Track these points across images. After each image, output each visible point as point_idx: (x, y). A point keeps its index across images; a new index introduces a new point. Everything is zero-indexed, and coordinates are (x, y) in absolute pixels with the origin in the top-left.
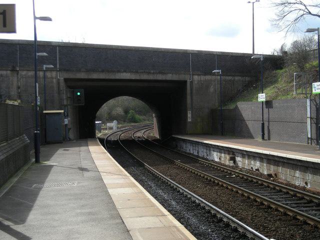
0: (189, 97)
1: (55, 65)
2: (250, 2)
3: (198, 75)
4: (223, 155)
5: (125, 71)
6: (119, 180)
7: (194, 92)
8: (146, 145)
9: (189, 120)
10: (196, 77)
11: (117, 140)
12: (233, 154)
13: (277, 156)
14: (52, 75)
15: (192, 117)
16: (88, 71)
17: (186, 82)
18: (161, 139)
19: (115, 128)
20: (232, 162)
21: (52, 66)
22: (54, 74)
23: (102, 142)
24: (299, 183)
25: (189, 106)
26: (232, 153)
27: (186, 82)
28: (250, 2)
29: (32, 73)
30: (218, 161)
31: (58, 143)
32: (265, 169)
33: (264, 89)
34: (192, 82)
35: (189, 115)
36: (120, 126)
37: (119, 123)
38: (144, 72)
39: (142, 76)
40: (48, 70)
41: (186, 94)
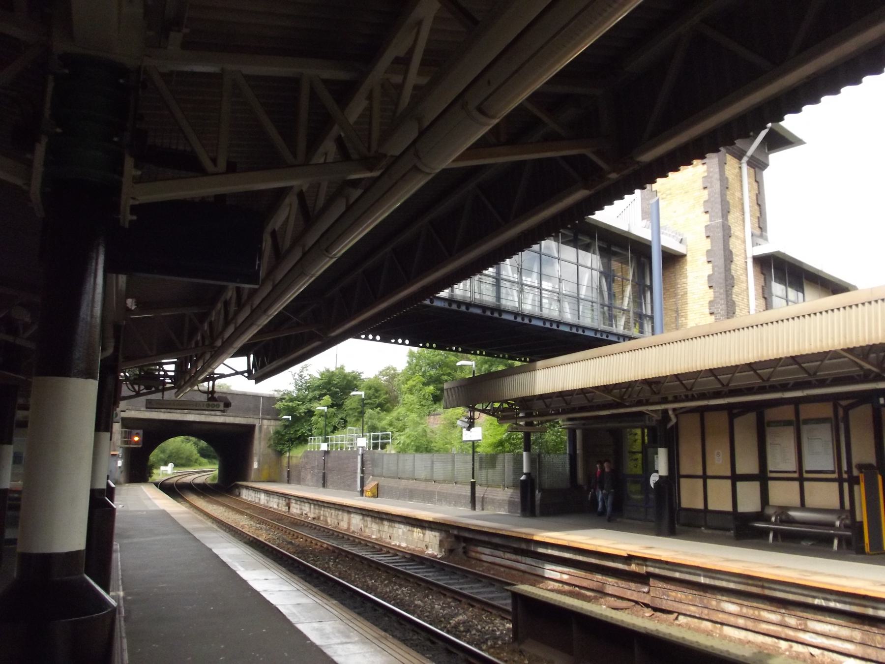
4: (281, 501)
8: (202, 490)
10: (265, 422)
24: (344, 525)
34: (261, 427)
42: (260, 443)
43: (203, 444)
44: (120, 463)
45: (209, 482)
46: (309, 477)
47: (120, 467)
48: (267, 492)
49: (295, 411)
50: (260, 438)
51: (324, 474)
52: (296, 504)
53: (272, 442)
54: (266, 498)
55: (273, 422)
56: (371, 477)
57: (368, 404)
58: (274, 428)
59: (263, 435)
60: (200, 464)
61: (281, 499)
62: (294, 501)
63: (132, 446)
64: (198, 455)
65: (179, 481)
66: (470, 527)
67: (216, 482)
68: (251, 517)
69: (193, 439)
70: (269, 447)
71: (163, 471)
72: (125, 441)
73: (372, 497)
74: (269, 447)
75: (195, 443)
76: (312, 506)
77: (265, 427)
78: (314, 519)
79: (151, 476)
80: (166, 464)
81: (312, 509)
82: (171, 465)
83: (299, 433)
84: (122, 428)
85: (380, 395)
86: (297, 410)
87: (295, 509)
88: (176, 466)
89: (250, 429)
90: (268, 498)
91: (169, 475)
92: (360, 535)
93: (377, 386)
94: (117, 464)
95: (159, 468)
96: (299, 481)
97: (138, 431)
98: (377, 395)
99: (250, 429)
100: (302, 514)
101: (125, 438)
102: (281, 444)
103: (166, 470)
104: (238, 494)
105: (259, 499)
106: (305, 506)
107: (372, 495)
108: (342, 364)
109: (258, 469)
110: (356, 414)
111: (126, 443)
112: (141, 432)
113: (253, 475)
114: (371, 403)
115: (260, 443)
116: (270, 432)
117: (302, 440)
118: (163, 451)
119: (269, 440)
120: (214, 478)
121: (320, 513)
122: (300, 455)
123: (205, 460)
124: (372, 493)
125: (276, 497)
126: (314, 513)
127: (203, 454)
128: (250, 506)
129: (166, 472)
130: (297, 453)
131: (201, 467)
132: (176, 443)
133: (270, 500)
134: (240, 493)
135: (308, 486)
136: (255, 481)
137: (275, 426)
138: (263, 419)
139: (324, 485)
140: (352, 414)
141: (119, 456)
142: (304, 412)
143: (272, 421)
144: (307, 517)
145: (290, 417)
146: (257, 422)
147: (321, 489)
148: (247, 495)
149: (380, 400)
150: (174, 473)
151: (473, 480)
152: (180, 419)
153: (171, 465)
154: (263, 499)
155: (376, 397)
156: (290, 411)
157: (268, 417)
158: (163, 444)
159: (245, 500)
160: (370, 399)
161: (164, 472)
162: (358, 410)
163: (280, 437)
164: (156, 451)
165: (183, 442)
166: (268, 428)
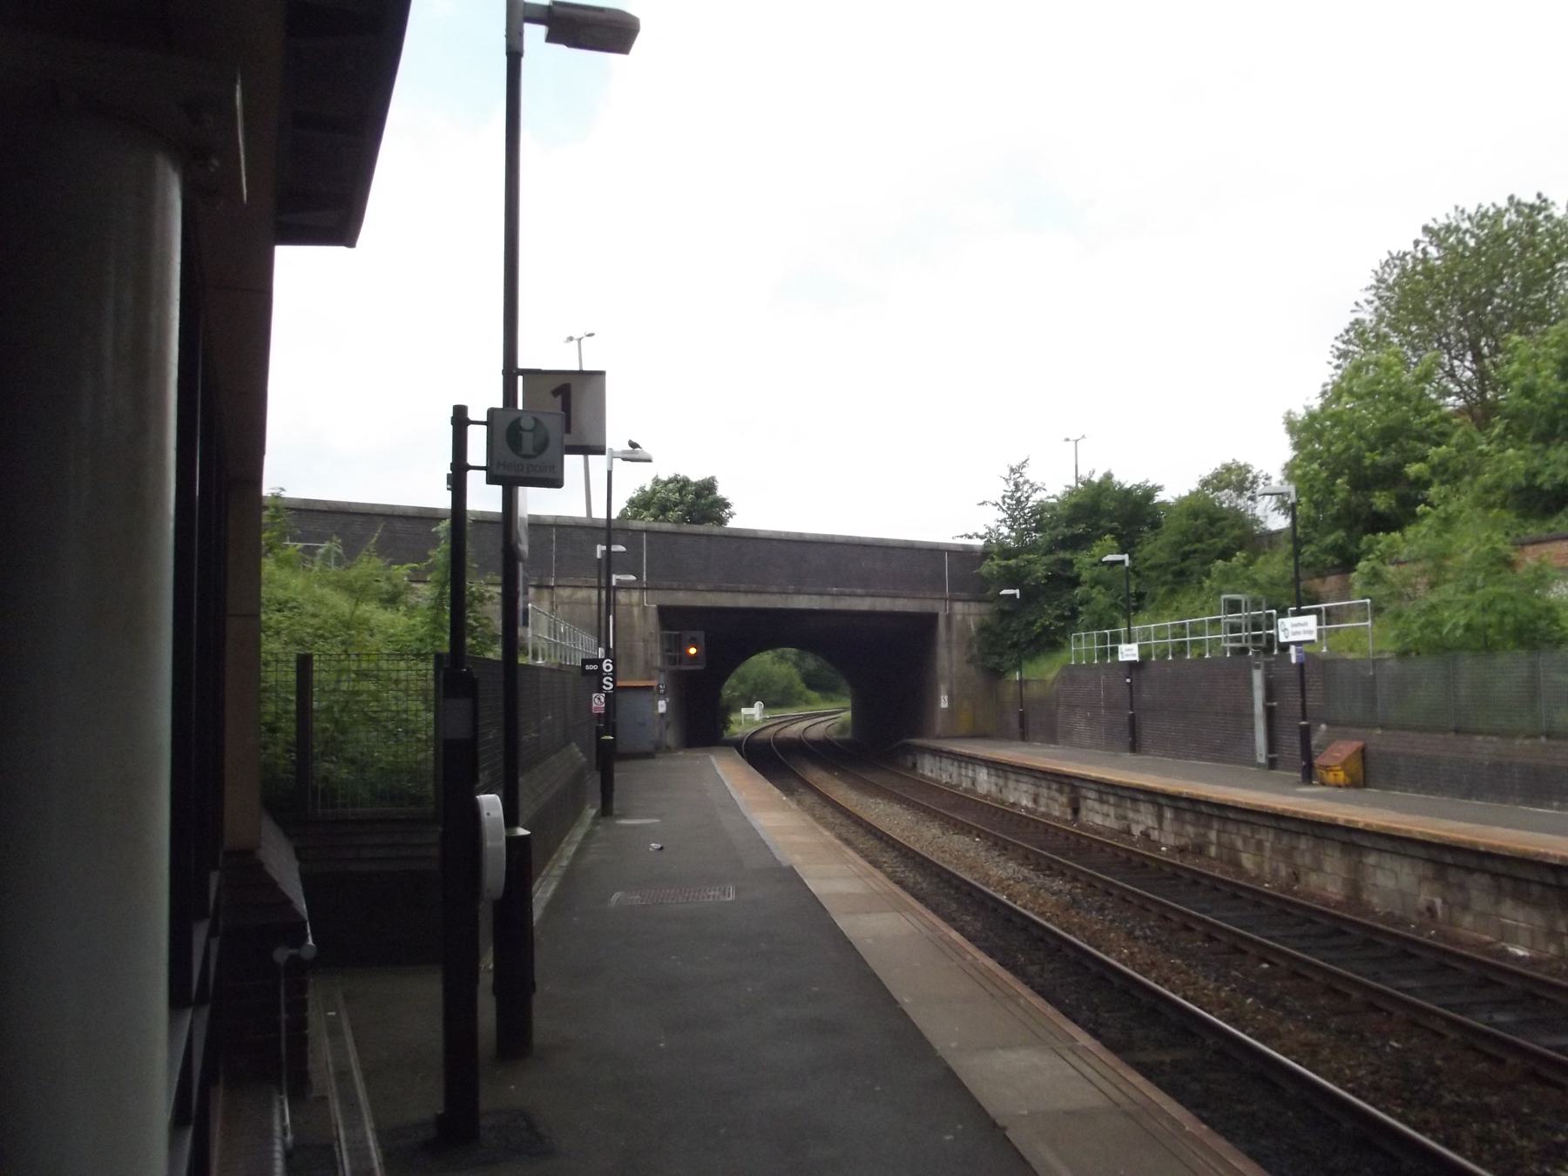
1: (639, 576)
2: (1067, 440)
3: (964, 601)
4: (1044, 791)
8: (825, 753)
10: (959, 607)
11: (769, 740)
12: (1074, 788)
17: (932, 618)
20: (1069, 811)
21: (633, 578)
22: (635, 596)
23: (736, 744)
24: (945, 778)
26: (1071, 785)
28: (1067, 440)
30: (1030, 805)
32: (1168, 836)
33: (938, 1055)
34: (949, 618)
40: (623, 586)
42: (950, 652)
43: (811, 662)
44: (662, 707)
45: (835, 737)
46: (1081, 727)
47: (662, 714)
48: (994, 766)
49: (1025, 577)
50: (949, 641)
51: (1132, 718)
52: (1101, 801)
53: (975, 651)
54: (993, 779)
55: (974, 607)
56: (1323, 726)
57: (1195, 551)
58: (977, 618)
59: (954, 637)
60: (808, 702)
61: (1044, 783)
62: (1092, 795)
63: (684, 668)
64: (804, 685)
65: (780, 736)
66: (1393, 833)
67: (848, 736)
68: (1026, 858)
69: (791, 652)
70: (969, 662)
71: (746, 715)
72: (670, 657)
73: (1347, 786)
74: (969, 662)
75: (796, 665)
76: (1168, 814)
77: (959, 617)
78: (1182, 850)
79: (726, 728)
80: (750, 705)
81: (1167, 824)
82: (758, 706)
83: (1036, 628)
84: (663, 629)
85: (1223, 529)
86: (1029, 574)
87: (1098, 816)
88: (767, 706)
89: (926, 622)
90: (1001, 782)
91: (757, 723)
92: (1445, 938)
93: (1211, 511)
94: (656, 707)
95: (740, 711)
96: (1051, 735)
97: (694, 634)
98: (1214, 530)
99: (926, 622)
100: (1128, 832)
101: (670, 651)
102: (994, 654)
103: (753, 715)
104: (910, 764)
105: (974, 781)
106: (1138, 811)
107: (1348, 781)
108: (1105, 470)
109: (950, 710)
110: (1170, 577)
111: (673, 661)
112: (700, 635)
113: (939, 725)
114: (1204, 551)
115: (950, 652)
116: (969, 628)
117: (1050, 642)
118: (743, 680)
119: (970, 646)
120: (843, 728)
121: (1205, 835)
122: (1051, 676)
123: (814, 695)
124: (1347, 774)
125: (1026, 779)
126: (1178, 834)
127: (812, 682)
128: (932, 788)
129: (752, 716)
130: (1044, 672)
131: (810, 708)
132: (764, 663)
133: (1006, 786)
134: (915, 765)
135: (1082, 747)
136: (946, 737)
137: (980, 614)
138: (953, 600)
139: (1134, 747)
140: (1158, 578)
141: (659, 689)
142: (1047, 577)
143: (972, 604)
144: (1156, 845)
145: (1017, 592)
146: (941, 609)
147: (1128, 756)
148: (929, 768)
149: (1226, 541)
150: (765, 720)
151: (1303, 723)
152: (780, 605)
153: (758, 706)
154: (984, 781)
155: (1213, 535)
156: (1013, 578)
157: (964, 595)
158: (741, 670)
159: (930, 779)
160: (1199, 540)
161: (748, 718)
162: (1174, 568)
163: (992, 639)
164: (732, 681)
165: (774, 664)
166: (964, 620)
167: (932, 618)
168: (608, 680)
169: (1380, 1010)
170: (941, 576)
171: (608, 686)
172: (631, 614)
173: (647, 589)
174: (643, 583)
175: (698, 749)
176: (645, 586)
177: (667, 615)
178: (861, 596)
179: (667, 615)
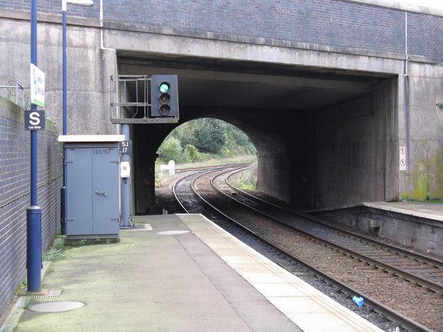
0: (401, 114)
5: (268, 44)
6: (96, 251)
7: (412, 100)
9: (402, 168)
10: (416, 69)
13: (407, 215)
14: (84, 39)
15: (408, 162)
16: (178, 35)
17: (395, 77)
18: (286, 200)
19: (172, 172)
22: (90, 35)
25: (401, 134)
27: (395, 77)
29: (25, 29)
31: (96, 243)
34: (407, 78)
35: (402, 156)
36: (179, 167)
37: (176, 163)
38: (311, 50)
39: (306, 57)
41: (396, 107)
77: (416, 80)
84: (119, 73)
94: (117, 171)
113: (402, 186)
157: (423, 59)
167: (389, 81)
168: (34, 116)
169: (389, 321)
170: (401, 36)
171: (35, 121)
172: (84, 58)
173: (103, 28)
174: (99, 22)
175: (225, 59)
176: (102, 25)
177: (126, 59)
178: (330, 53)
179: (126, 59)
